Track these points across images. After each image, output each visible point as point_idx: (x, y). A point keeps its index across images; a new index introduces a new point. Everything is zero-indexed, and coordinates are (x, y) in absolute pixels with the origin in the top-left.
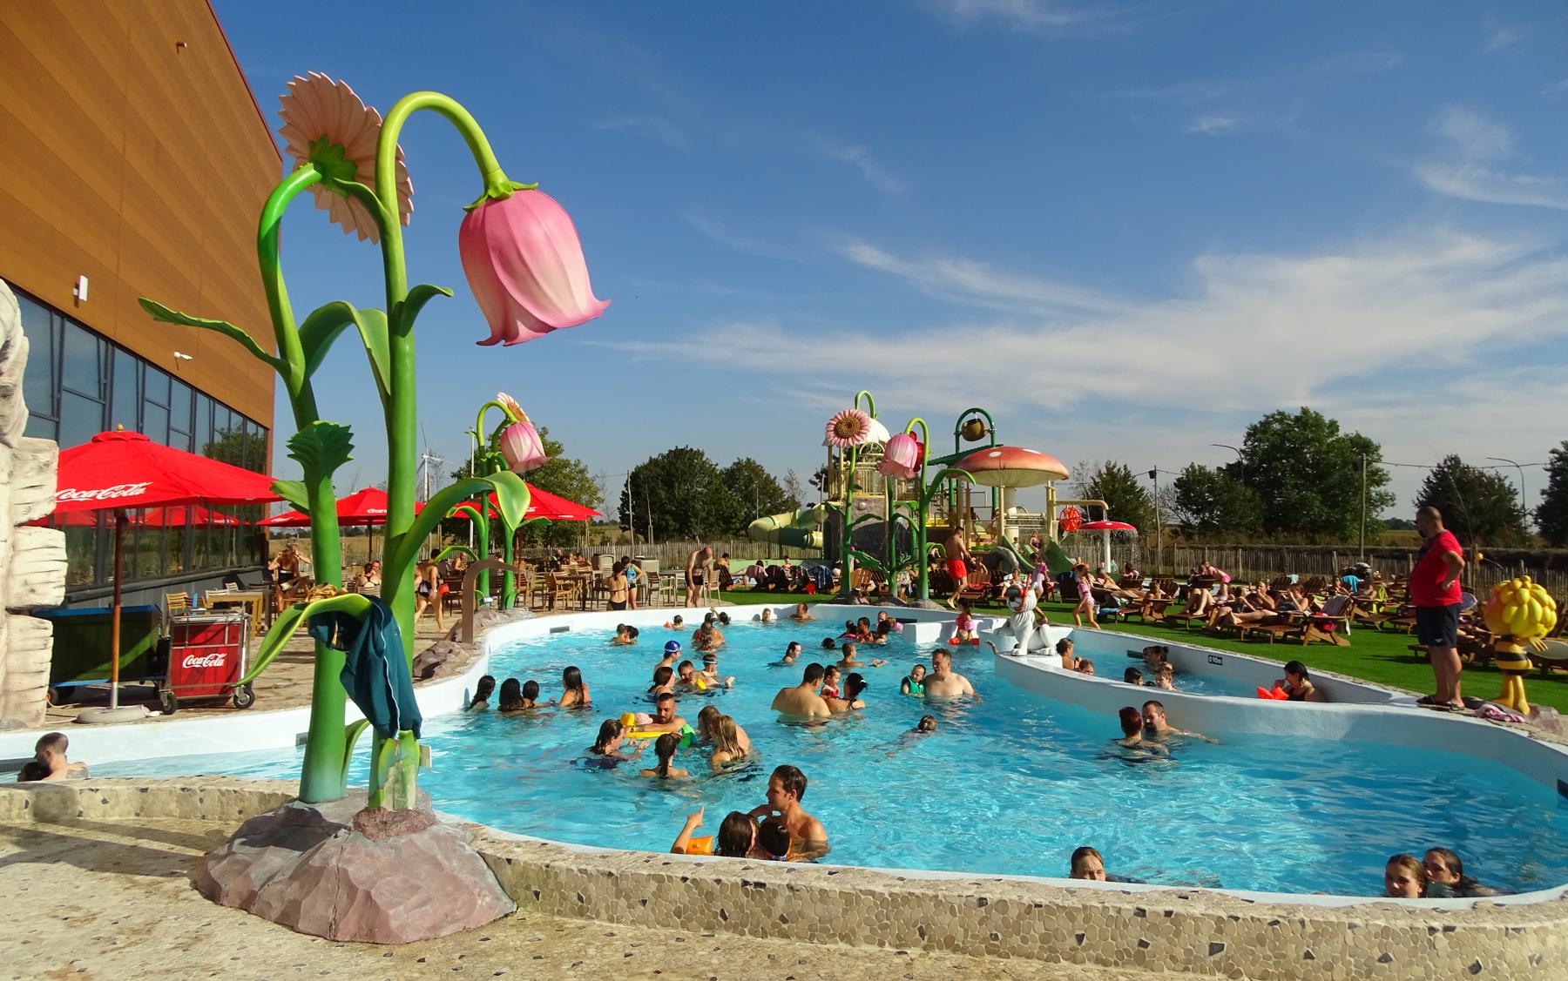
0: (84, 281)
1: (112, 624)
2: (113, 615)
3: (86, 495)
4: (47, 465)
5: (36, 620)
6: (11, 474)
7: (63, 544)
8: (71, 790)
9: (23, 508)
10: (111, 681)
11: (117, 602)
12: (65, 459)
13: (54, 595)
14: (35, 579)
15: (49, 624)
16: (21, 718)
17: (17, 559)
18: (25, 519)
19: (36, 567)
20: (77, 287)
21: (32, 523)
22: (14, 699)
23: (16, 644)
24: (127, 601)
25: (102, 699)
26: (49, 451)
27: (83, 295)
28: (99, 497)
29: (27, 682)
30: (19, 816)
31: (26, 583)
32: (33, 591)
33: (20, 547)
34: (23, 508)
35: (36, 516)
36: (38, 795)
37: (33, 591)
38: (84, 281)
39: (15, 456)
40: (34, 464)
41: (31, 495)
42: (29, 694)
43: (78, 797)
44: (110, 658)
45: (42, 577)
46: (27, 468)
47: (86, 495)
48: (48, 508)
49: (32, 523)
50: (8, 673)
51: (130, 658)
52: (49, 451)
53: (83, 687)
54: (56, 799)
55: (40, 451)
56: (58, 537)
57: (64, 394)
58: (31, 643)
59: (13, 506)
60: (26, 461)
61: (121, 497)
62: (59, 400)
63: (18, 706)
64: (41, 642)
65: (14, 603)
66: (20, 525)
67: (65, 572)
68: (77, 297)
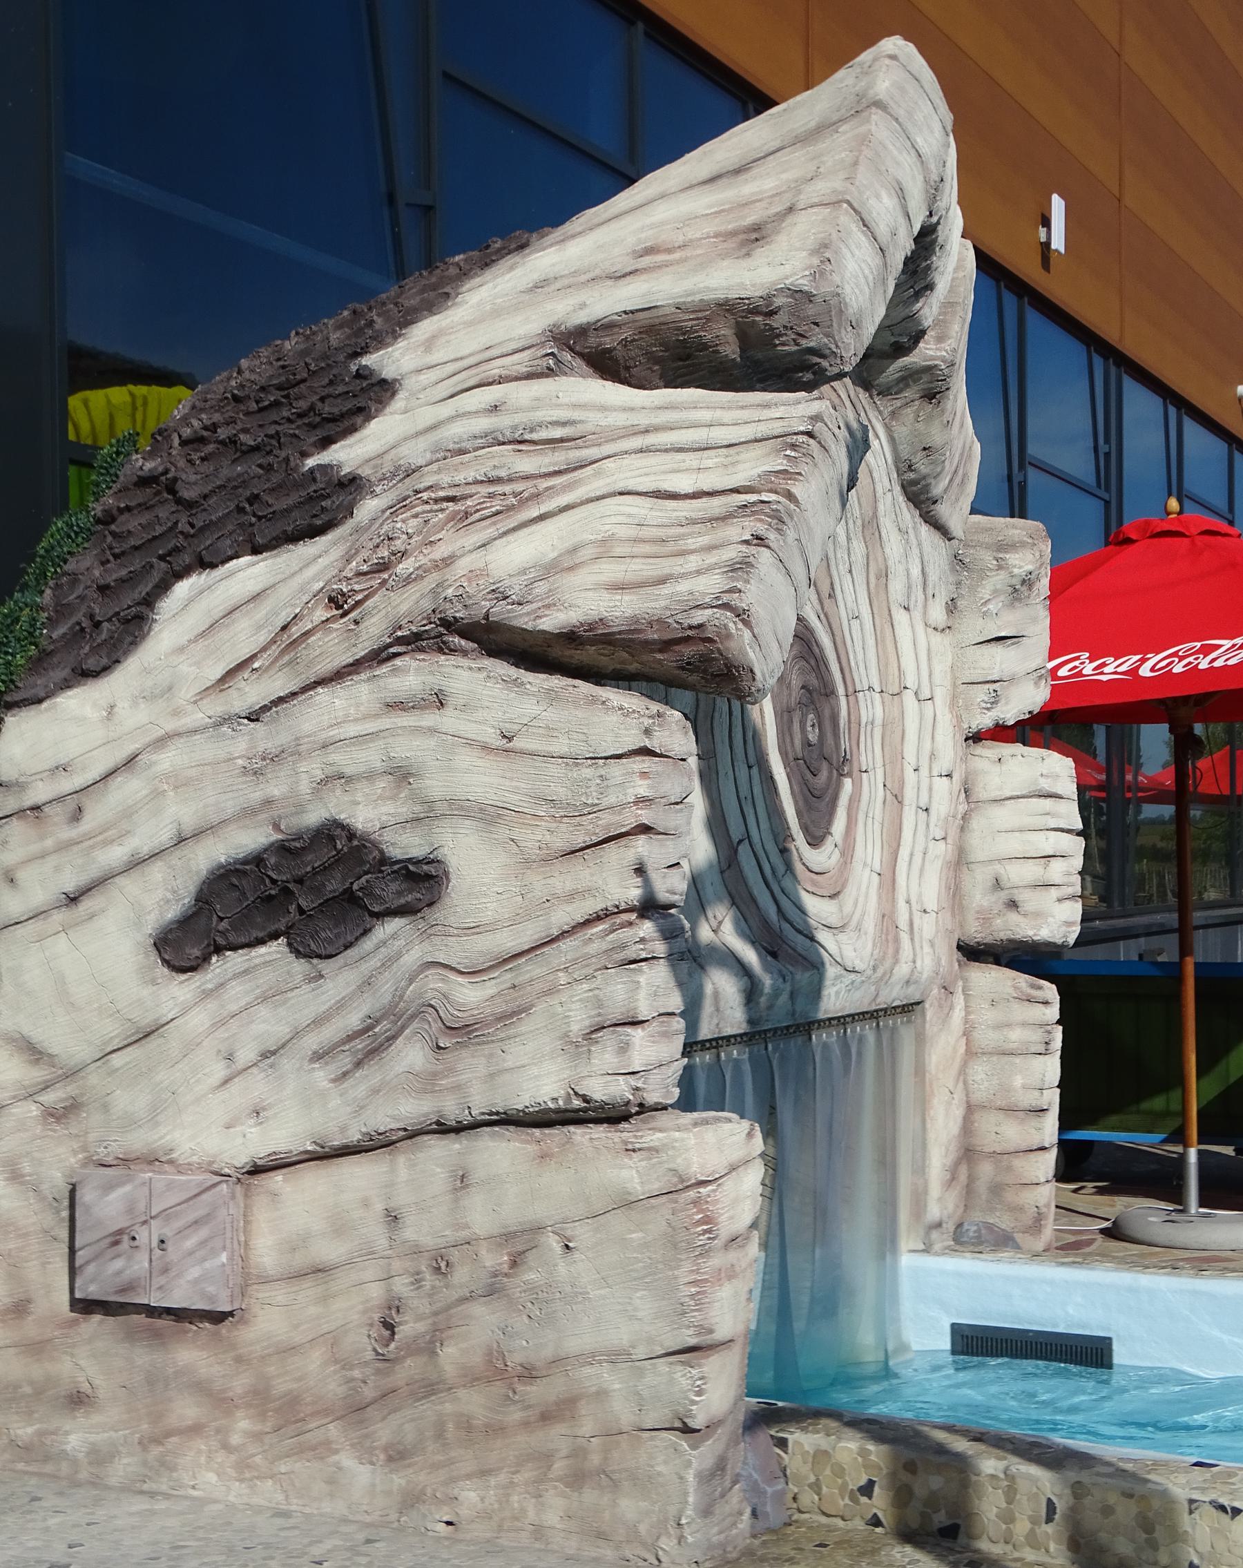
0: (1058, 206)
1: (1176, 997)
2: (1180, 979)
3: (1114, 668)
4: (1028, 582)
5: (1023, 980)
6: (952, 607)
7: (1069, 788)
8: (1164, 1494)
9: (981, 694)
10: (1186, 1145)
11: (1185, 949)
12: (1066, 583)
13: (1057, 919)
14: (1020, 874)
15: (1050, 991)
16: (1004, 1221)
17: (976, 823)
18: (986, 721)
19: (1013, 844)
20: (1046, 222)
21: (1001, 733)
22: (986, 1170)
23: (986, 1038)
24: (1207, 948)
25: (1162, 1182)
26: (1028, 550)
27: (1058, 243)
28: (1145, 671)
29: (1013, 1133)
30: (1033, 1541)
31: (997, 884)
32: (1013, 905)
33: (981, 793)
34: (981, 694)
35: (1013, 710)
36: (1078, 1491)
37: (1013, 905)
38: (1058, 206)
39: (958, 561)
40: (998, 580)
41: (1000, 660)
42: (1018, 1163)
43: (1186, 1522)
44: (1180, 1081)
45: (1032, 871)
46: (985, 592)
47: (1114, 668)
48: (1030, 697)
49: (1001, 733)
50: (970, 1109)
51: (1214, 1087)
52: (1028, 550)
53: (1110, 1144)
54: (1126, 1512)
55: (1012, 547)
56: (1056, 769)
57: (1031, 472)
58: (1016, 1036)
59: (963, 685)
60: (982, 574)
61: (1193, 671)
62: (1023, 487)
63: (997, 1189)
64: (1036, 1036)
65: (976, 933)
66: (976, 738)
67: (1078, 862)
68: (1047, 245)
